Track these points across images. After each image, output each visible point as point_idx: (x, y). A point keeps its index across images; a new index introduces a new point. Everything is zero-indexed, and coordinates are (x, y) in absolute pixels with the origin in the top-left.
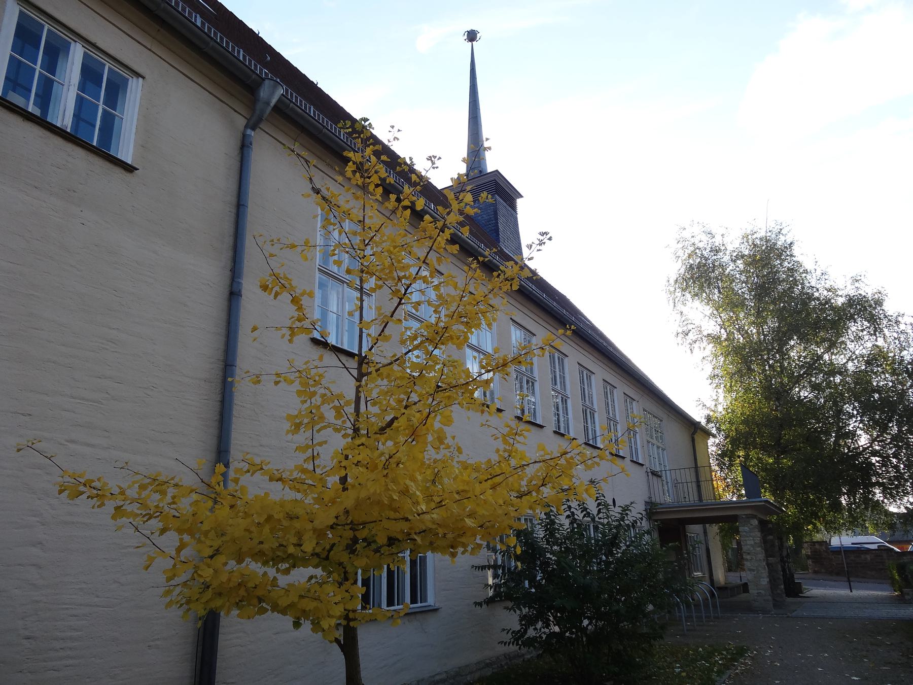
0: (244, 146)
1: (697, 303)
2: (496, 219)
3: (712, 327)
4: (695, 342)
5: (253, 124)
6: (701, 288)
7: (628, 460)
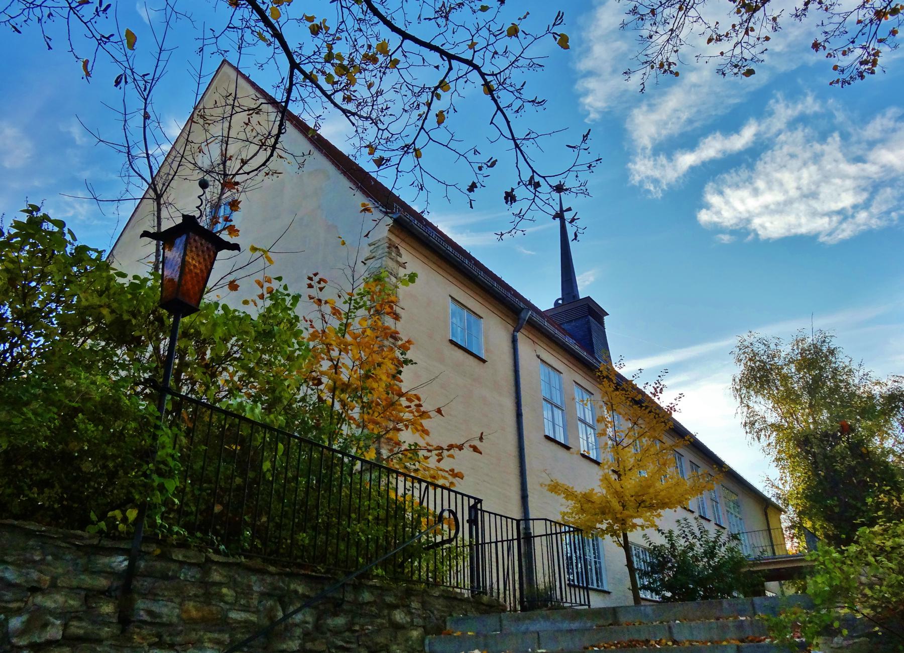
0: (514, 341)
1: (760, 398)
4: (761, 430)
5: (517, 330)
6: (762, 386)
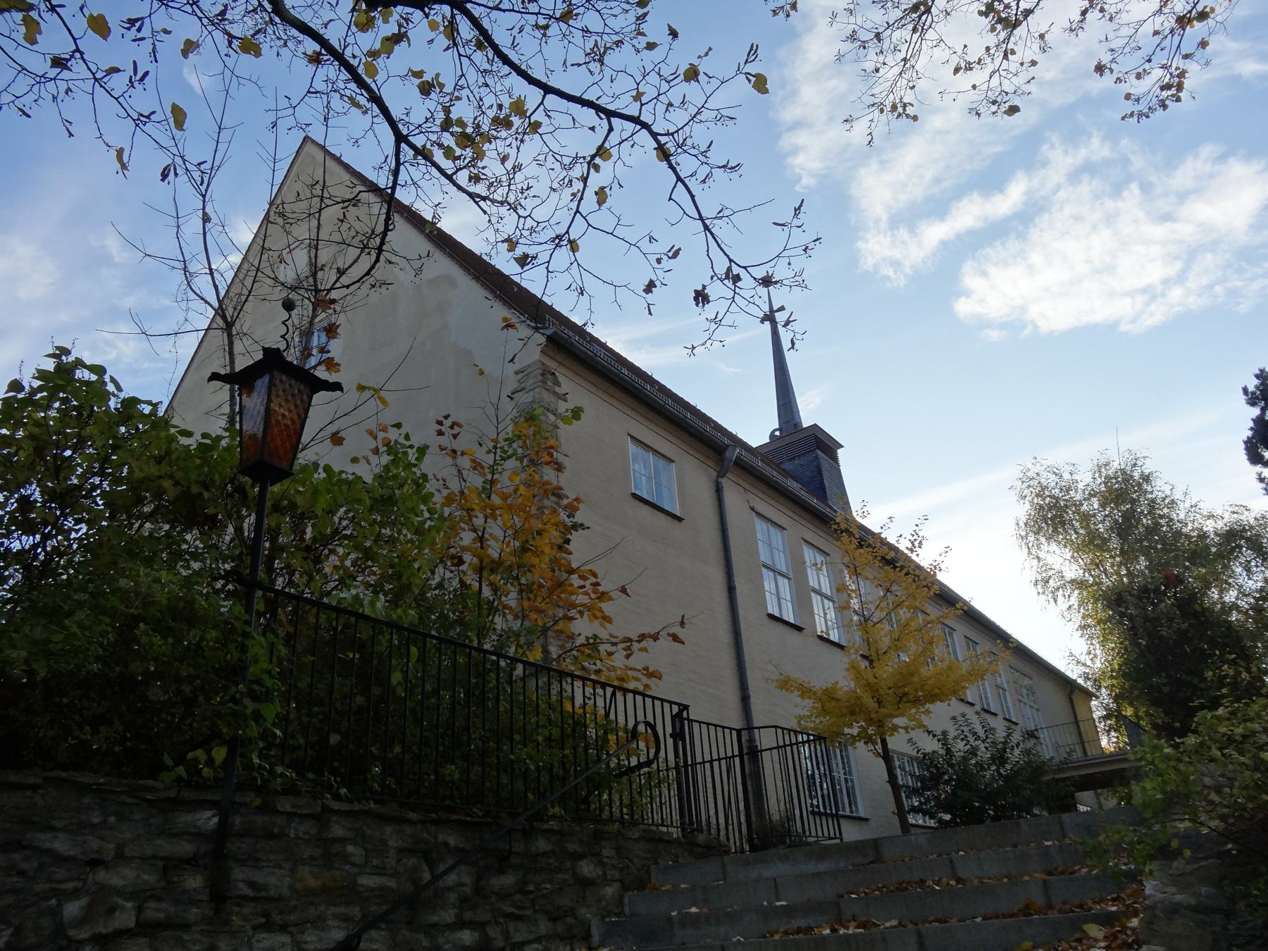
0: (719, 490)
2: (821, 475)
3: (1073, 571)
4: (1058, 589)
5: (721, 474)
7: (1000, 717)
